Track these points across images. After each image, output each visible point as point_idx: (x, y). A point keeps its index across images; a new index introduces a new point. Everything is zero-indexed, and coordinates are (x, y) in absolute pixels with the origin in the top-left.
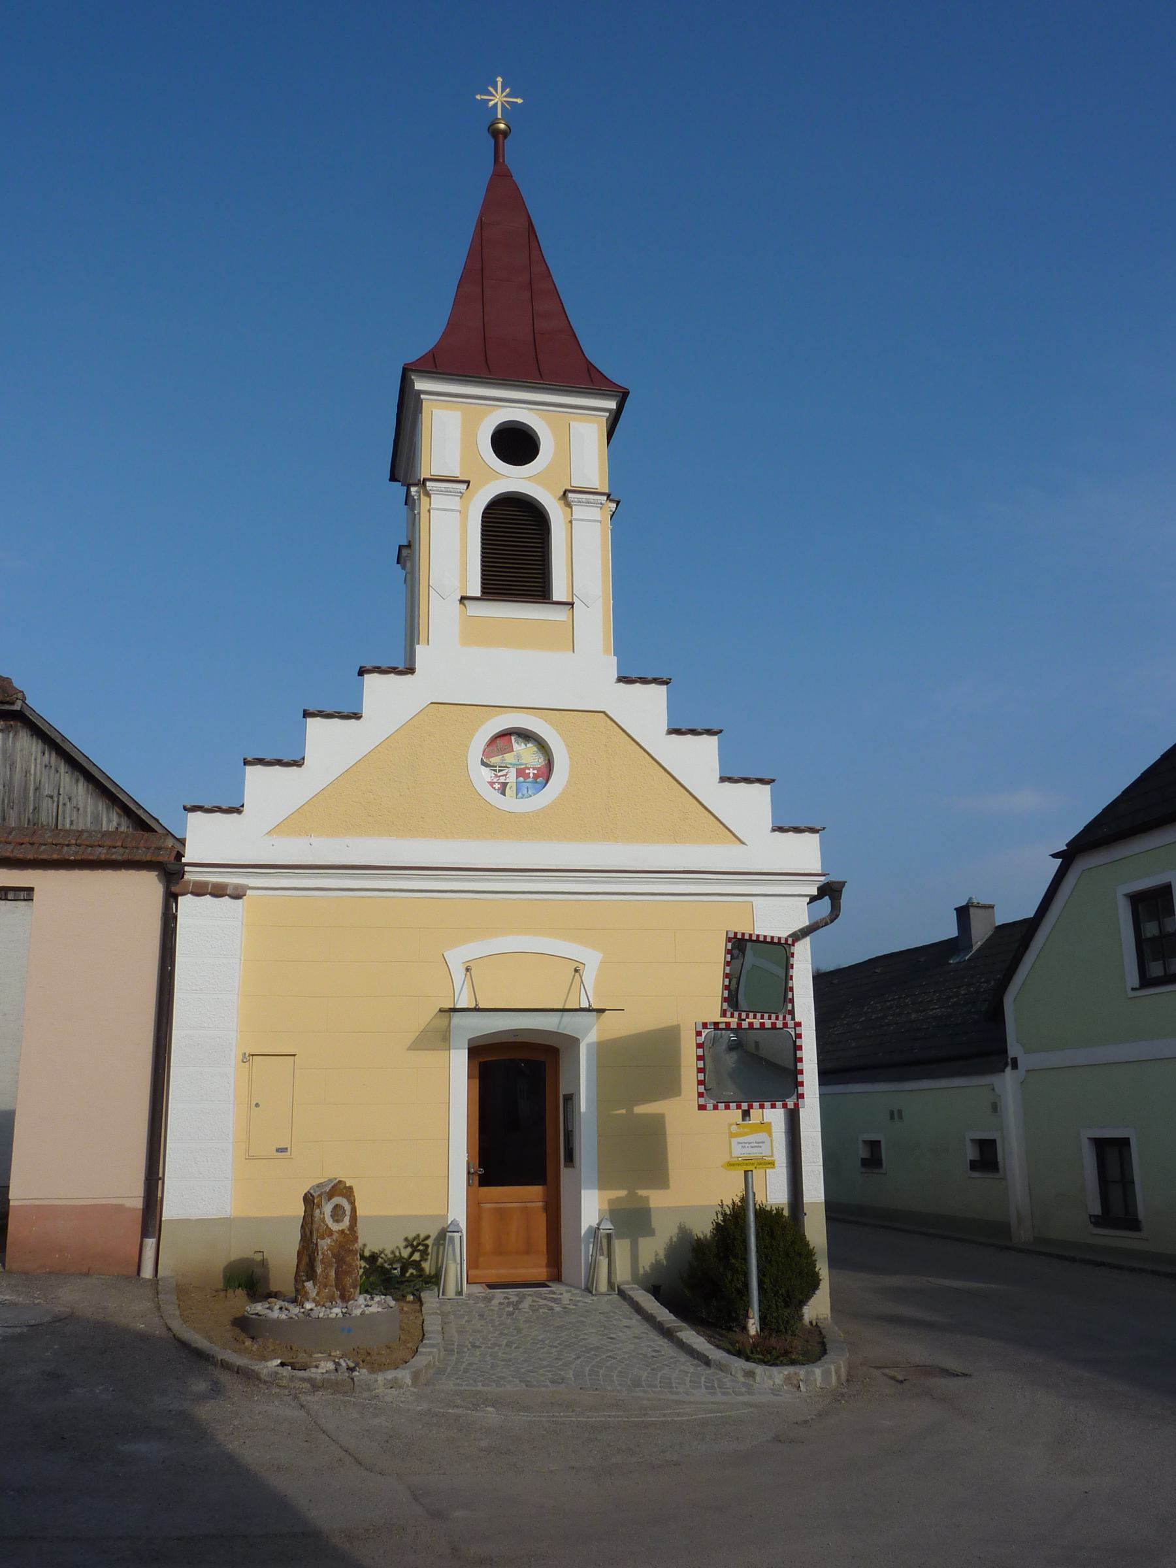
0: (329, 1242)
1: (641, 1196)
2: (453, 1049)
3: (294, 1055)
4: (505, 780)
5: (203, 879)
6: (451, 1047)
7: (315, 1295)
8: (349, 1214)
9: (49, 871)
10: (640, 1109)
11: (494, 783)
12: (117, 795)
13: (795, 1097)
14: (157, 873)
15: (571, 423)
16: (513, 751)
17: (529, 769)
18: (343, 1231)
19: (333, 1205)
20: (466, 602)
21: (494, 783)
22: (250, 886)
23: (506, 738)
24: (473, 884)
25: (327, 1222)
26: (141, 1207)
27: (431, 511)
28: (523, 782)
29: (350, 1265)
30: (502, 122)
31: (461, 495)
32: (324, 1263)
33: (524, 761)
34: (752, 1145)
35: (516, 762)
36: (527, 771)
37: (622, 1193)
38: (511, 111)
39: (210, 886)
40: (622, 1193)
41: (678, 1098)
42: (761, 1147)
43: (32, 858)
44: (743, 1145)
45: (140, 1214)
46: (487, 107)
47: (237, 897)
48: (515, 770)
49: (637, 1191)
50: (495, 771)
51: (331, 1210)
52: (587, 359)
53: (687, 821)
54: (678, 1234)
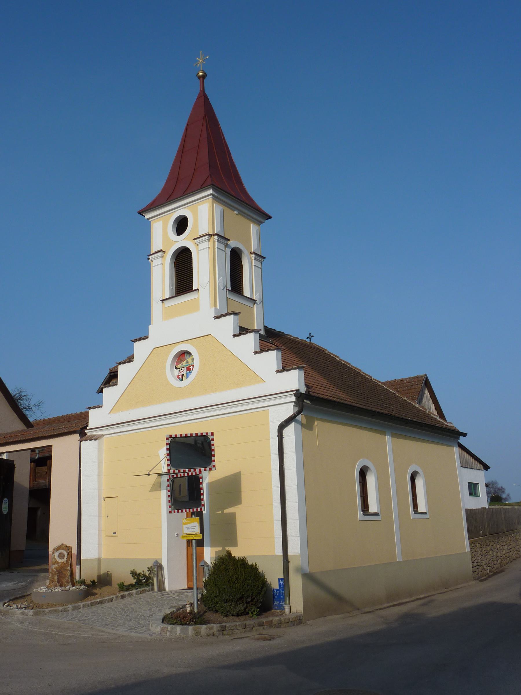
0: (56, 566)
3: (117, 497)
7: (48, 584)
8: (67, 556)
9: (13, 445)
10: (226, 511)
11: (179, 375)
17: (190, 366)
18: (63, 562)
19: (59, 553)
21: (179, 375)
22: (103, 434)
23: (183, 355)
25: (56, 559)
28: (189, 373)
29: (65, 575)
31: (163, 257)
32: (52, 573)
34: (191, 528)
37: (220, 549)
39: (296, 414)
40: (220, 549)
41: (240, 506)
42: (194, 529)
44: (188, 528)
50: (180, 370)
51: (58, 554)
53: (243, 376)
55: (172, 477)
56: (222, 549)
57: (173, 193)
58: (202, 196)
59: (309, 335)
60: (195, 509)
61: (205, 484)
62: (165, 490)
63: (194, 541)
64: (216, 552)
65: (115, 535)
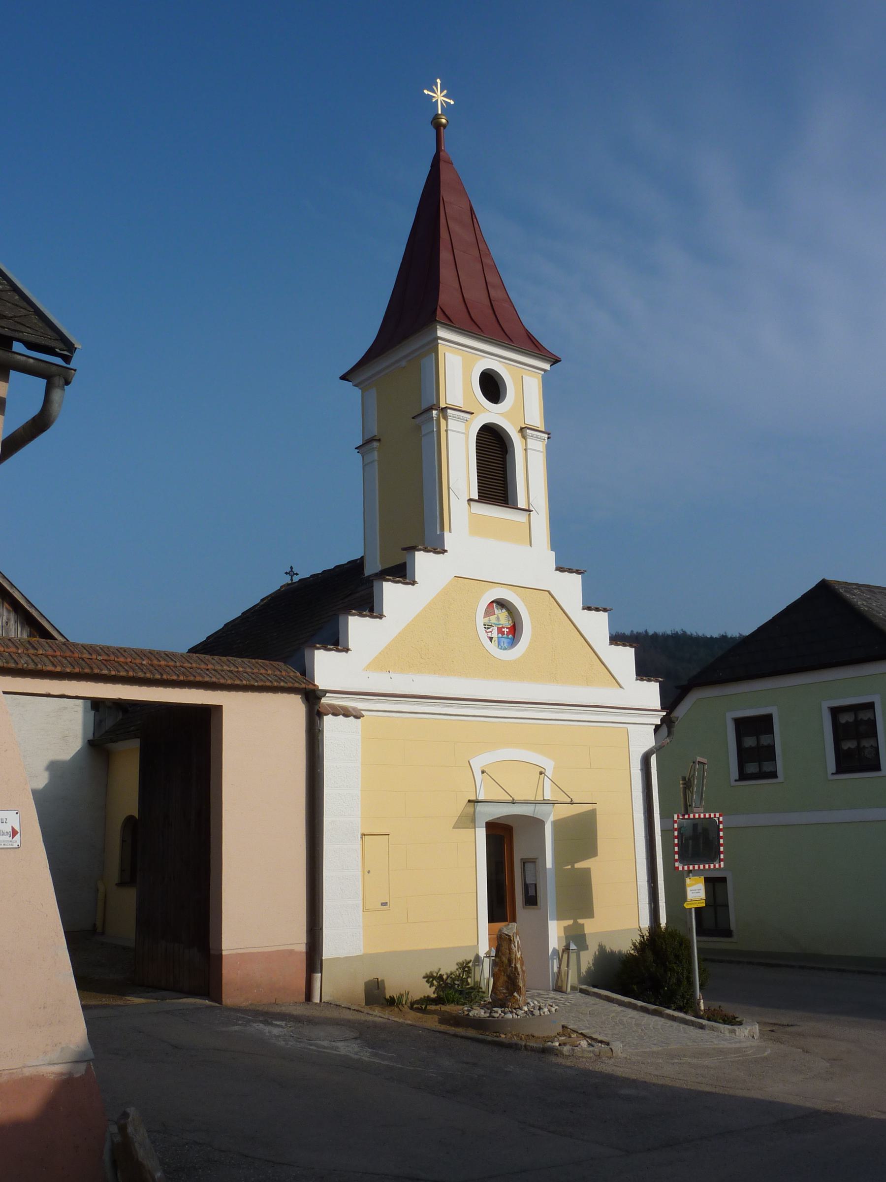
1: (580, 924)
2: (478, 827)
3: (388, 835)
4: (491, 635)
5: (331, 702)
6: (476, 826)
10: (578, 865)
12: (13, 593)
13: (718, 861)
14: (300, 696)
15: (524, 377)
16: (495, 614)
17: (504, 628)
20: (472, 503)
24: (496, 711)
26: (305, 951)
27: (449, 431)
30: (444, 117)
33: (501, 623)
35: (496, 622)
36: (503, 630)
37: (571, 922)
38: (447, 108)
40: (571, 922)
43: (230, 683)
45: (304, 955)
46: (432, 101)
47: (357, 717)
48: (497, 628)
49: (578, 920)
50: (485, 628)
52: (524, 327)
54: (598, 949)
55: (682, 817)
56: (573, 923)
57: (471, 317)
58: (526, 362)
59: (290, 570)
60: (690, 866)
61: (550, 822)
62: (484, 827)
63: (693, 910)
64: (565, 928)
65: (385, 907)
